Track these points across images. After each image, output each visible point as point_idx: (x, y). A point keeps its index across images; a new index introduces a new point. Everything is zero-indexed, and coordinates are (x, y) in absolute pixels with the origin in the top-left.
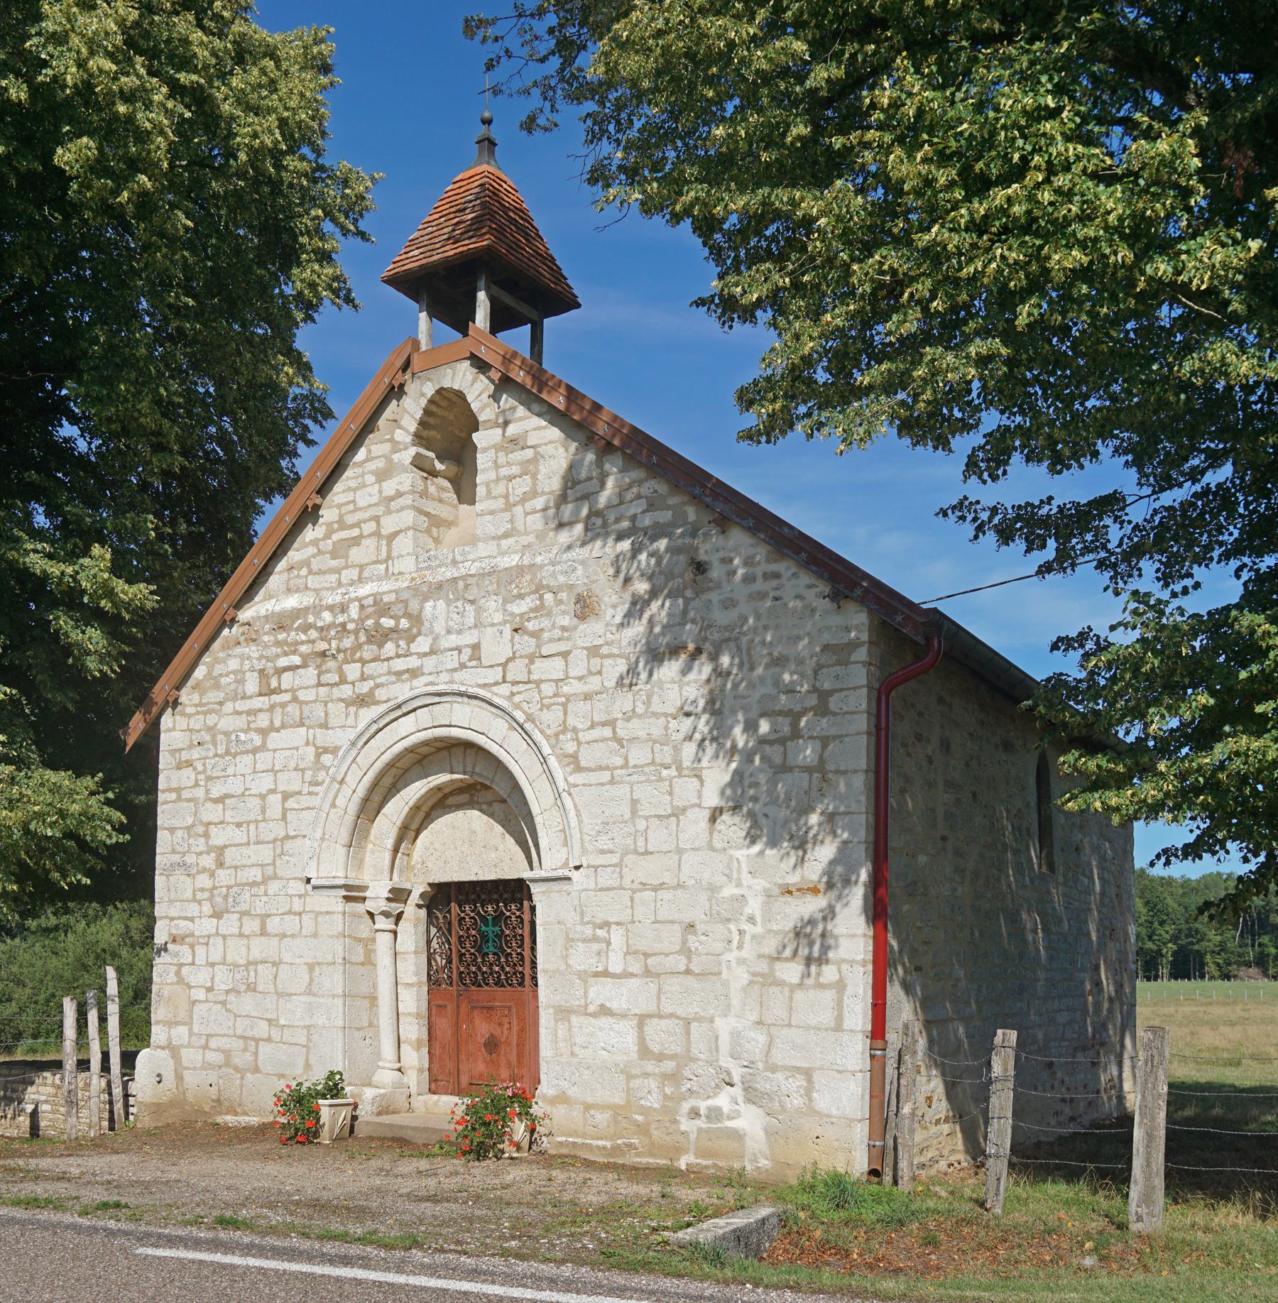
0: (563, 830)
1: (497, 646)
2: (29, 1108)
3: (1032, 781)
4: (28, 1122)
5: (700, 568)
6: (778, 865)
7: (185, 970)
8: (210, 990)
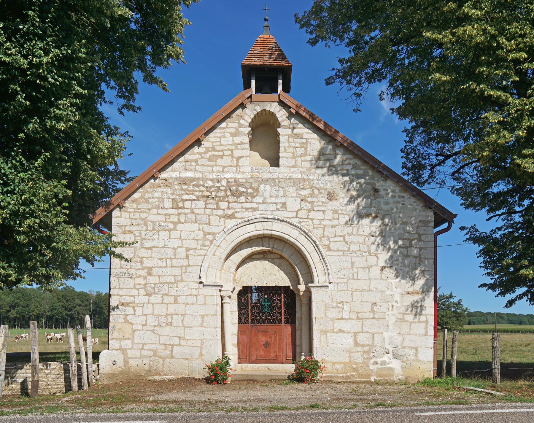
1: (293, 204)
4: (19, 387)
5: (376, 191)
6: (405, 285)
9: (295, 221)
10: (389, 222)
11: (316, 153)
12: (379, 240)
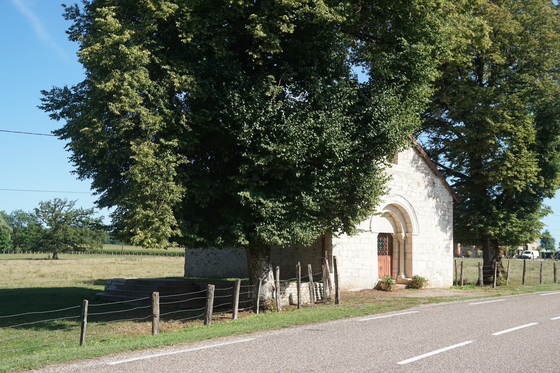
0: (406, 223)
1: (405, 188)
2: (288, 295)
3: (84, 339)
4: (288, 300)
5: (434, 183)
6: (444, 234)
7: (341, 252)
8: (347, 257)
9: (405, 197)
10: (159, 9)
11: (412, 159)
12: (435, 210)
